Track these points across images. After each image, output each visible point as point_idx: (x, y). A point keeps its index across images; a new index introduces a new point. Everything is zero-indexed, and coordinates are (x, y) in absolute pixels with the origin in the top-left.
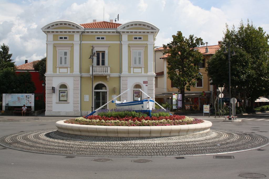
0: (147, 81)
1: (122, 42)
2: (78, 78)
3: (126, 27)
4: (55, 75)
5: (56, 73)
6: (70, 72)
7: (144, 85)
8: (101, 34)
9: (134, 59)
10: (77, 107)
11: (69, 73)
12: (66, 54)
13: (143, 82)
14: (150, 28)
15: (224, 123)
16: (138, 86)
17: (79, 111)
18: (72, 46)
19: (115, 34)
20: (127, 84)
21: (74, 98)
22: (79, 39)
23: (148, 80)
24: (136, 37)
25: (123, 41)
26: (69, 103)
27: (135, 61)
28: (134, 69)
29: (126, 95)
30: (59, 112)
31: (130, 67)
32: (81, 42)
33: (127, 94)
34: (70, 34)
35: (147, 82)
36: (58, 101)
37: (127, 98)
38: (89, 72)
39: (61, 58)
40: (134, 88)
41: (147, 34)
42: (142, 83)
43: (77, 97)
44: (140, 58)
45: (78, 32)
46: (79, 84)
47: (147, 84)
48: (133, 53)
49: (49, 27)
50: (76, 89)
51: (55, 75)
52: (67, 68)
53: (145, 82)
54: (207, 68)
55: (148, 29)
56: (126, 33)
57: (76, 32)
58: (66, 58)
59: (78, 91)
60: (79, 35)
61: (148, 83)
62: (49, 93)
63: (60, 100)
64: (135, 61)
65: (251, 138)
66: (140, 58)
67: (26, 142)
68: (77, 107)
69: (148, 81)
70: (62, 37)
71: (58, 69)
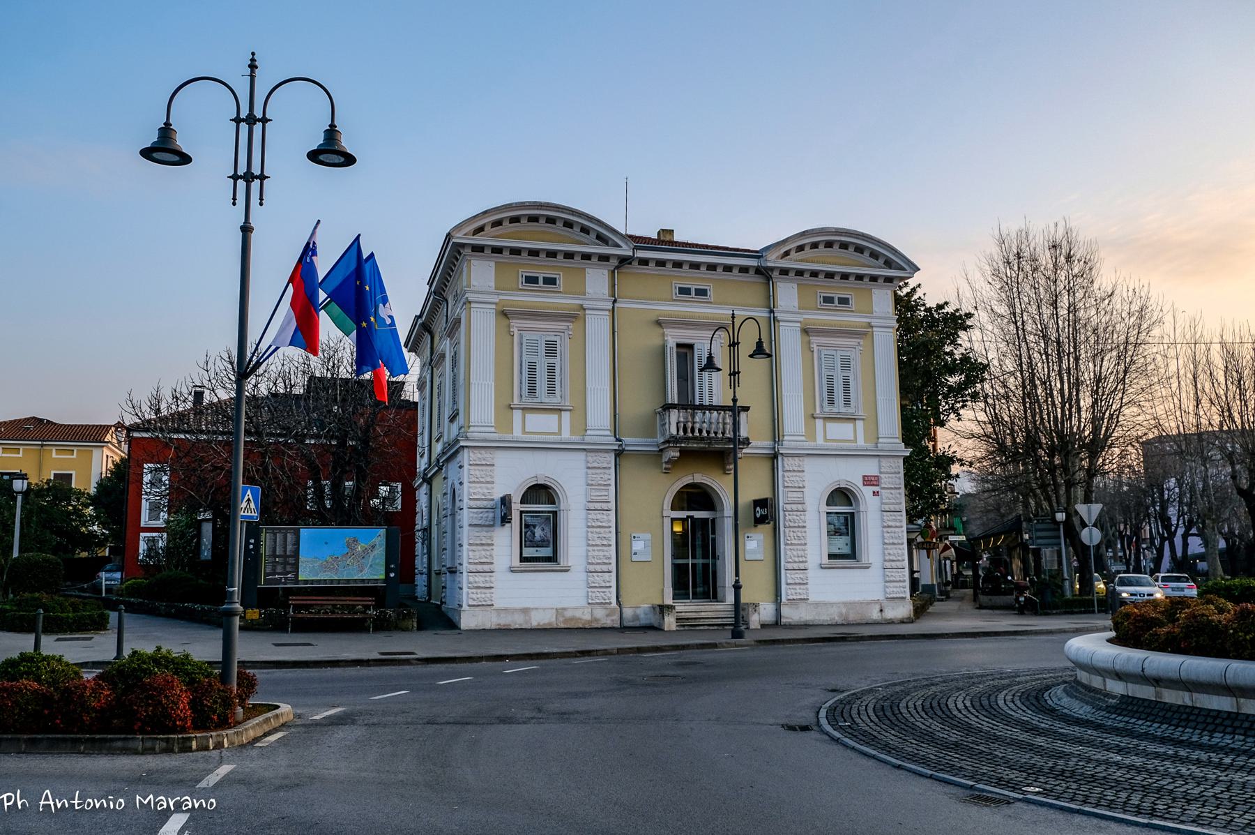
0: (878, 477)
1: (778, 312)
2: (608, 459)
3: (487, 229)
4: (836, 450)
6: (572, 433)
7: (868, 491)
9: (825, 381)
11: (861, 442)
12: (551, 349)
13: (864, 480)
14: (881, 261)
15: (1048, 641)
16: (842, 495)
17: (610, 603)
19: (751, 277)
20: (804, 487)
22: (605, 290)
23: (881, 473)
25: (472, 288)
27: (831, 392)
29: (800, 534)
30: (525, 611)
32: (615, 301)
33: (804, 527)
35: (878, 481)
36: (516, 562)
37: (805, 544)
39: (532, 367)
40: (828, 504)
42: (860, 483)
43: (605, 542)
44: (846, 382)
45: (604, 258)
46: (609, 485)
47: (876, 489)
48: (820, 359)
49: (787, 254)
51: (836, 450)
52: (855, 419)
53: (869, 481)
57: (595, 259)
58: (551, 370)
59: (608, 515)
60: (606, 272)
62: (480, 522)
63: (523, 559)
64: (831, 392)
65: (947, 705)
66: (846, 382)
67: (986, 725)
69: (882, 475)
70: (554, 276)
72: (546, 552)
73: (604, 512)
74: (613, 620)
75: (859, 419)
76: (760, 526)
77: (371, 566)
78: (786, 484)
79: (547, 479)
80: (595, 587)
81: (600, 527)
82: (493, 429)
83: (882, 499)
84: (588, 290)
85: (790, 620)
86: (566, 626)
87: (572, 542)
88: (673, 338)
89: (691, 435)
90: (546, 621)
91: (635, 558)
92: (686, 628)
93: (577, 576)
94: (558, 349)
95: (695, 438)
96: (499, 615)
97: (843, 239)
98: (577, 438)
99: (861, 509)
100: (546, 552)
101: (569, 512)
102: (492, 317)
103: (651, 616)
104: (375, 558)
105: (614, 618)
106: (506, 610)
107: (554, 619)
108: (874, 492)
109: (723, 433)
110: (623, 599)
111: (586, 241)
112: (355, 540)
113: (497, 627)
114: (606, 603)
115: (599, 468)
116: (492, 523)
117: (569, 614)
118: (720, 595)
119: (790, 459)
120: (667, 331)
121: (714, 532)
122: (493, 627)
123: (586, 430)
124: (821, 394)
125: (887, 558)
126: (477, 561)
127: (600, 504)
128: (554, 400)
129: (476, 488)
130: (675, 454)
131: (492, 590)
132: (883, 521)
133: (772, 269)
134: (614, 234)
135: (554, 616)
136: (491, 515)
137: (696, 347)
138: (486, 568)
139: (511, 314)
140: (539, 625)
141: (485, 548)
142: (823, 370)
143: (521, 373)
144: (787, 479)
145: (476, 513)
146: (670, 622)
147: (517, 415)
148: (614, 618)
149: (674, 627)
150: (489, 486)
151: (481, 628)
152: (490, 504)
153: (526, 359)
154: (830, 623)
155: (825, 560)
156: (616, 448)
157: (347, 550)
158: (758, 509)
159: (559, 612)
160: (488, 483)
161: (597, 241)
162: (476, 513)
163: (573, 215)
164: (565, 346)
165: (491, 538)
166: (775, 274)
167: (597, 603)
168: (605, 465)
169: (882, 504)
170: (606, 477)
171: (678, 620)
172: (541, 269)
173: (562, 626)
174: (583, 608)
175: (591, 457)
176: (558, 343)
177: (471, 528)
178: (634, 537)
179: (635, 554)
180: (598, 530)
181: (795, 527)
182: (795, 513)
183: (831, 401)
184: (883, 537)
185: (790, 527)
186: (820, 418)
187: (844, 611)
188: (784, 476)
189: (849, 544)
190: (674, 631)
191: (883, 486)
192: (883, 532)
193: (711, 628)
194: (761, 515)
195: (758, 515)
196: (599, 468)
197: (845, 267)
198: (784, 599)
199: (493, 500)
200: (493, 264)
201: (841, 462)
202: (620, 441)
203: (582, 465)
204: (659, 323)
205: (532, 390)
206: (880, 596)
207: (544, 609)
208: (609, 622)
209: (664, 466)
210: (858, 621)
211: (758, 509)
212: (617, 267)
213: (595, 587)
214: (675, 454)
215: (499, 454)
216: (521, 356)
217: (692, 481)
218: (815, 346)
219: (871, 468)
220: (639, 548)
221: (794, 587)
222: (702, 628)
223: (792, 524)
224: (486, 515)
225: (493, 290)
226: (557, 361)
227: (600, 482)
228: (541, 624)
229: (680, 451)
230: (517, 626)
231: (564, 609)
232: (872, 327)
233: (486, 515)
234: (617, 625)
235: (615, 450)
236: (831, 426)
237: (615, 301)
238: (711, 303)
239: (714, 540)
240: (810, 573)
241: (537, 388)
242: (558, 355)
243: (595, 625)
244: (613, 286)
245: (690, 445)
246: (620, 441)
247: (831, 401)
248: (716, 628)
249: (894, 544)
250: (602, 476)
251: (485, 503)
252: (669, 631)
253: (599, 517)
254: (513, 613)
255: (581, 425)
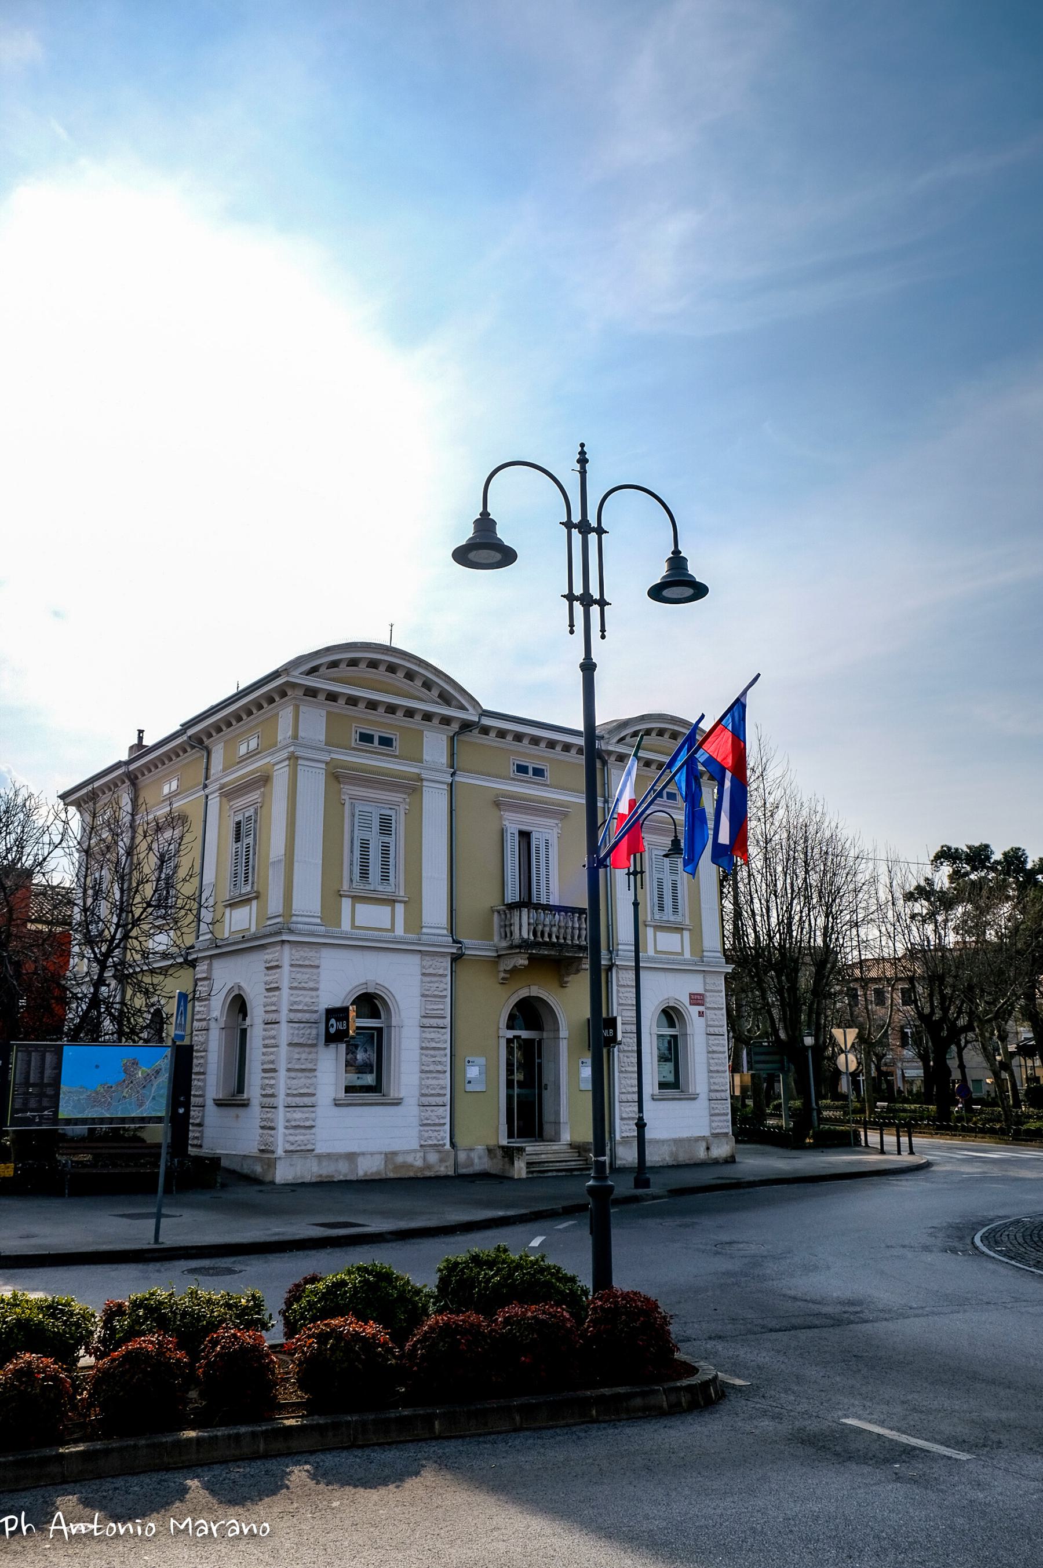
5: (339, 924)
7: (694, 1010)
8: (533, 750)
10: (435, 1125)
11: (400, 931)
13: (690, 998)
14: (435, 693)
18: (412, 787)
21: (424, 1075)
22: (444, 759)
24: (384, 749)
26: (397, 1103)
27: (661, 897)
28: (358, 906)
30: (351, 1157)
31: (332, 896)
34: (408, 723)
38: (489, 936)
39: (365, 846)
41: (421, 728)
42: (686, 1001)
44: (385, 851)
45: (446, 721)
47: (701, 1008)
49: (314, 670)
50: (434, 1022)
52: (394, 901)
53: (696, 999)
54: (365, 1288)
55: (421, 695)
56: (322, 697)
60: (445, 737)
61: (708, 1000)
62: (301, 1041)
64: (661, 897)
68: (435, 1125)
69: (708, 994)
70: (527, 764)
71: (346, 904)
72: (369, 1079)
73: (439, 1030)
74: (447, 1167)
75: (686, 929)
76: (333, 1046)
77: (154, 1098)
78: (621, 1002)
79: (378, 987)
80: (429, 1125)
81: (434, 1048)
82: (319, 921)
83: (706, 1020)
84: (425, 757)
85: (624, 1162)
86: (398, 1176)
87: (404, 1067)
88: (514, 823)
89: (541, 940)
90: (374, 1169)
91: (469, 1088)
92: (535, 1175)
93: (410, 1111)
94: (393, 826)
95: (545, 944)
96: (320, 1162)
97: (676, 728)
98: (411, 936)
99: (688, 1032)
100: (369, 1079)
101: (402, 1029)
102: (322, 778)
103: (486, 1159)
104: (159, 1088)
105: (448, 1164)
106: (329, 1156)
107: (382, 1167)
108: (699, 1012)
109: (572, 940)
110: (457, 1139)
111: (424, 697)
112: (135, 1063)
113: (318, 1179)
114: (440, 1145)
115: (434, 975)
116: (315, 1042)
117: (400, 1159)
118: (548, 1129)
119: (624, 972)
120: (507, 815)
121: (540, 1057)
122: (314, 1180)
123: (703, 951)
124: (652, 899)
125: (712, 1088)
126: (295, 1092)
127: (437, 1020)
128: (389, 889)
129: (298, 996)
130: (522, 961)
131: (313, 1131)
132: (708, 1045)
133: (610, 753)
134: (461, 695)
135: (383, 1163)
136: (314, 1032)
137: (534, 836)
138: (307, 1100)
139: (344, 777)
140: (366, 1175)
141: (307, 1074)
142: (356, 832)
143: (352, 852)
144: (621, 995)
145: (298, 1029)
146: (520, 1169)
147: (346, 904)
148: (448, 1164)
149: (524, 1175)
150: (314, 993)
151: (300, 1181)
152: (315, 1016)
153: (656, 875)
154: (661, 1164)
155: (342, 1094)
156: (455, 951)
157: (123, 1076)
158: (333, 1021)
159: (390, 1156)
160: (312, 989)
161: (438, 700)
162: (298, 1029)
163: (419, 665)
164: (400, 825)
165: (315, 1061)
166: (612, 759)
167: (431, 1146)
168: (441, 972)
169: (707, 1026)
170: (442, 986)
171: (529, 1164)
172: (378, 724)
173: (391, 1175)
174: (415, 1151)
175: (428, 961)
176: (393, 818)
177: (291, 1048)
178: (469, 1062)
179: (469, 1082)
180: (432, 1052)
181: (629, 1051)
182: (629, 1035)
183: (661, 908)
184: (709, 1065)
185: (624, 1051)
186: (346, 896)
187: (674, 1149)
188: (618, 991)
189: (673, 1072)
190: (523, 1179)
191: (708, 1005)
192: (708, 1058)
193: (560, 1174)
194: (338, 1030)
195: (332, 1030)
196: (434, 975)
197: (659, 755)
198: (618, 1138)
199: (316, 1012)
200: (324, 713)
201: (670, 976)
202: (460, 943)
203: (416, 970)
204: (497, 804)
205: (364, 874)
206: (707, 1134)
207: (372, 1154)
208: (442, 1169)
209: (502, 975)
210: (688, 1162)
211: (333, 1021)
212: (457, 734)
213: (429, 1125)
214: (522, 961)
215: (325, 953)
216: (352, 831)
217: (528, 995)
218: (346, 797)
219: (696, 984)
220: (473, 1076)
221: (628, 1122)
222: (550, 1174)
223: (626, 1048)
224: (308, 1031)
225: (322, 745)
226: (391, 840)
227: (436, 993)
228: (369, 1173)
229: (528, 958)
230: (341, 1178)
231: (395, 1154)
232: (422, 780)
233: (308, 1031)
234: (451, 1173)
235: (453, 953)
236: (362, 908)
237: (453, 774)
238: (395, 757)
239: (540, 1065)
240: (319, 1110)
241: (370, 872)
242: (393, 832)
243: (428, 1174)
244: (452, 755)
245: (541, 952)
246: (460, 943)
247: (364, 874)
248: (564, 1173)
249: (718, 1072)
250: (437, 985)
251: (307, 1016)
252: (520, 1179)
253: (433, 1036)
254: (337, 1159)
255: (414, 921)
